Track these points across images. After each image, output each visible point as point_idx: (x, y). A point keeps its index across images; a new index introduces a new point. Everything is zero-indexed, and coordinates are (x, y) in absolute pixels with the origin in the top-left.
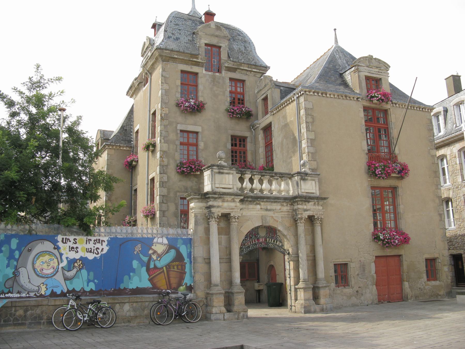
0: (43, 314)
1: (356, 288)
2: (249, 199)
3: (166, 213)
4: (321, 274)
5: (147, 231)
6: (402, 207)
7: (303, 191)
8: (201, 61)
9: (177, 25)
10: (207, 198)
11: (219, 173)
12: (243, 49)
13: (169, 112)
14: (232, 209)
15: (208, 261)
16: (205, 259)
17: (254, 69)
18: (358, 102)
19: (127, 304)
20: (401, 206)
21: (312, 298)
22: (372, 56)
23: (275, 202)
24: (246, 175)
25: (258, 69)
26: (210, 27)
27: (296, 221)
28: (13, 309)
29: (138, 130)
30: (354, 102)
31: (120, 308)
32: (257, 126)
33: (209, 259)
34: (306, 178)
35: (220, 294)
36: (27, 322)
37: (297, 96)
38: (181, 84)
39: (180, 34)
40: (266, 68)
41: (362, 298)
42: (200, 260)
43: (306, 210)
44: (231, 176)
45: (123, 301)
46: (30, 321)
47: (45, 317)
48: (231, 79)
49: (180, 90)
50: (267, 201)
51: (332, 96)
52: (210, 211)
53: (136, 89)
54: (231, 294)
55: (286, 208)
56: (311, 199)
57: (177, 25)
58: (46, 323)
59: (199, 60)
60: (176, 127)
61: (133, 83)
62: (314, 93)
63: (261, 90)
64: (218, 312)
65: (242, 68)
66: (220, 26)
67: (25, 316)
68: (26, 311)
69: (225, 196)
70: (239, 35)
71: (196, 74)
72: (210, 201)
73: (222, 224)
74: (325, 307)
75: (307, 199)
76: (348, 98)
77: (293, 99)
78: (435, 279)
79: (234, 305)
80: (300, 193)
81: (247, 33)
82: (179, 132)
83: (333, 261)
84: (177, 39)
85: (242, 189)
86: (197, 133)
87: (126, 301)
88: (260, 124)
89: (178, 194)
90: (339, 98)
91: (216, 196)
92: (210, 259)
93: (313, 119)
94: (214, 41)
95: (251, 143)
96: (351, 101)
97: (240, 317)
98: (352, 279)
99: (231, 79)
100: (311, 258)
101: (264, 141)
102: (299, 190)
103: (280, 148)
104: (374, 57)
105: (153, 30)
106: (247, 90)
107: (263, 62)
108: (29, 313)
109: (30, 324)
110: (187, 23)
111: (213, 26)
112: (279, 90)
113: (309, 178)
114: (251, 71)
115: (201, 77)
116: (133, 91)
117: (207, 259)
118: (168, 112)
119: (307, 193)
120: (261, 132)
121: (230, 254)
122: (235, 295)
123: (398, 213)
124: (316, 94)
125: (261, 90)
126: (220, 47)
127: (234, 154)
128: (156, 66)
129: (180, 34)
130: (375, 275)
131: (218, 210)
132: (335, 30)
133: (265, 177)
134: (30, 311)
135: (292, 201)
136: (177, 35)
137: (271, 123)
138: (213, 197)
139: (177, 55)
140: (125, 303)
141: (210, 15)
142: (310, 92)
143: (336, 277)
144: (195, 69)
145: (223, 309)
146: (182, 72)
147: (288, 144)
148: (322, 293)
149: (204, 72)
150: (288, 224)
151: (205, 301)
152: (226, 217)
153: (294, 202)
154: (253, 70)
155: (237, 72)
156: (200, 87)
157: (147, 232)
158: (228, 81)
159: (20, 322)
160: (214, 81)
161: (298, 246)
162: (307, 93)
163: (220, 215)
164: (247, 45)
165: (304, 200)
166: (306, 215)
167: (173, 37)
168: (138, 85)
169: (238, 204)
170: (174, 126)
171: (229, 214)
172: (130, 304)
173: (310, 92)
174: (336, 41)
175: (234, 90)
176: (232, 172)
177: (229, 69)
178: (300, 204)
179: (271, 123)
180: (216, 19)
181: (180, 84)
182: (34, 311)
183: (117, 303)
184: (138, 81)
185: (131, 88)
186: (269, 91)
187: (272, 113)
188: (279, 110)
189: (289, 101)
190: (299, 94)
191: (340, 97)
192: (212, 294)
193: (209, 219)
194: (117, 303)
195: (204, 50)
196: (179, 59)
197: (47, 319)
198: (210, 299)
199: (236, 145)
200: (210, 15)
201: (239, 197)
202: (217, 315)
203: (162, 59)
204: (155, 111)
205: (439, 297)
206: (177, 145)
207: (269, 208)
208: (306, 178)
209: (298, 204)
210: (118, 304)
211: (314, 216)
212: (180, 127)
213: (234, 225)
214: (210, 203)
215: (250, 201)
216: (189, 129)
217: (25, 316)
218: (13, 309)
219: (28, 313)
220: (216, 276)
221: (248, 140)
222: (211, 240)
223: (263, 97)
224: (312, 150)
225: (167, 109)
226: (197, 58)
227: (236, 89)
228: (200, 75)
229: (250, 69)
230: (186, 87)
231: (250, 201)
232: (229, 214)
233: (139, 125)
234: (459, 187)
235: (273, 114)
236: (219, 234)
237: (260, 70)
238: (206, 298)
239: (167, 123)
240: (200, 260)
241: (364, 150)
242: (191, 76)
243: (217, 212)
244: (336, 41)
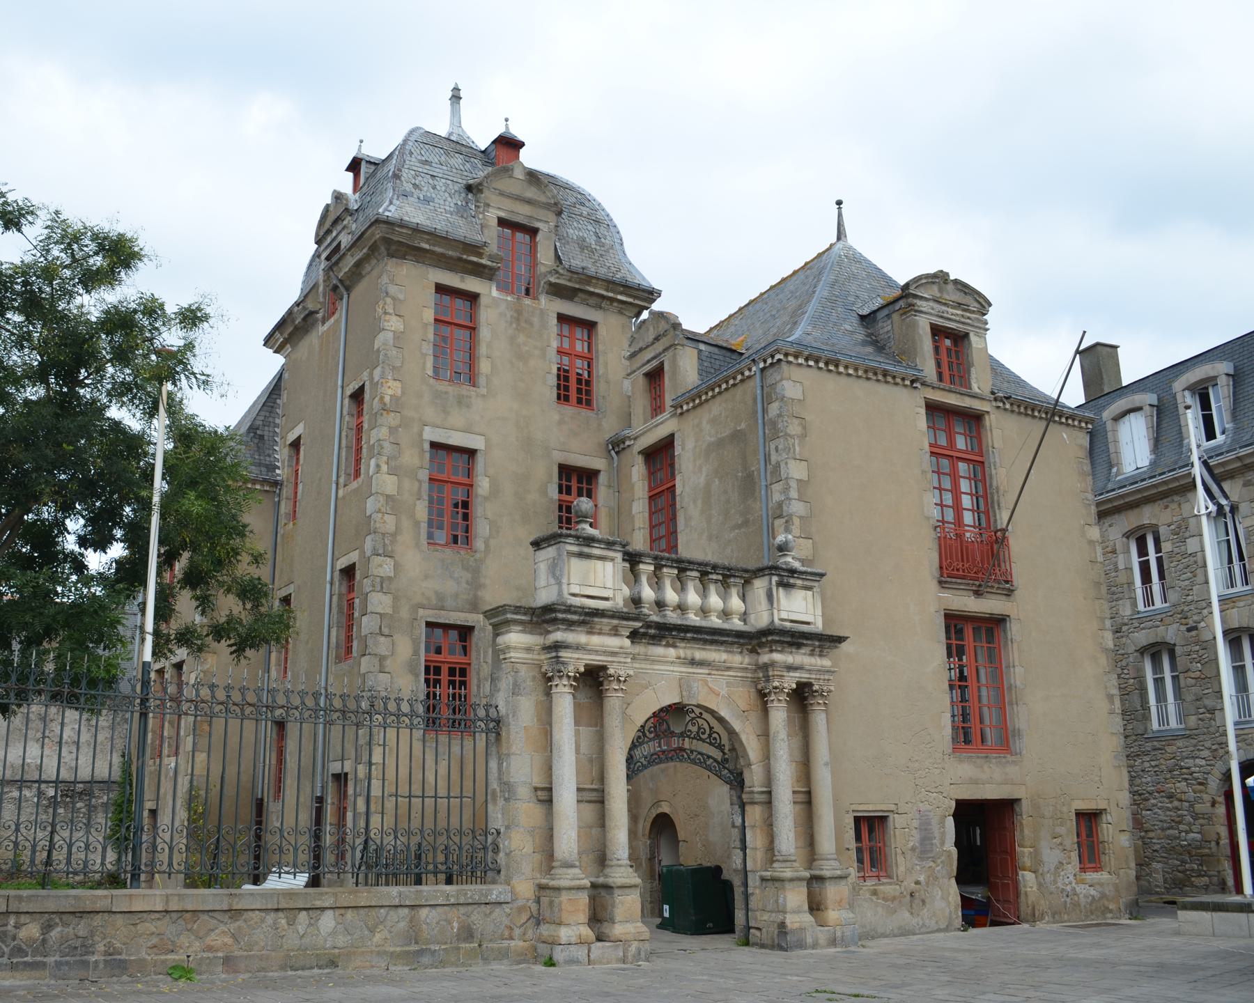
0: (97, 938)
1: (909, 884)
2: (656, 631)
3: (388, 662)
4: (826, 844)
5: (398, 705)
6: (1019, 670)
7: (784, 615)
8: (489, 263)
9: (426, 162)
10: (547, 622)
11: (581, 555)
12: (592, 240)
13: (403, 393)
14: (613, 654)
15: (546, 796)
16: (536, 789)
17: (621, 293)
18: (916, 393)
19: (329, 913)
20: (1017, 670)
21: (806, 907)
22: (947, 274)
23: (712, 642)
24: (641, 566)
25: (631, 296)
26: (511, 177)
27: (765, 695)
28: (12, 921)
29: (299, 437)
30: (905, 391)
31: (310, 925)
32: (627, 443)
33: (550, 789)
34: (792, 581)
35: (579, 888)
36: (51, 960)
37: (762, 365)
38: (436, 320)
39: (434, 188)
40: (651, 294)
41: (925, 912)
42: (524, 792)
43: (790, 668)
44: (609, 565)
45: (318, 904)
46: (57, 958)
47: (101, 947)
48: (562, 318)
49: (431, 336)
50: (693, 639)
51: (851, 371)
52: (558, 657)
53: (296, 328)
54: (603, 893)
55: (738, 659)
56: (807, 639)
57: (426, 162)
58: (101, 966)
59: (484, 261)
60: (421, 435)
61: (290, 312)
62: (807, 359)
63: (641, 350)
64: (573, 940)
65: (592, 289)
66: (533, 177)
67: (44, 941)
68: (47, 928)
69: (596, 619)
70: (582, 204)
71: (473, 298)
72: (558, 629)
73: (584, 697)
74: (839, 934)
75: (795, 638)
76: (889, 379)
77: (747, 373)
78: (1097, 869)
79: (613, 921)
80: (776, 620)
81: (599, 199)
82: (427, 446)
83: (854, 807)
84: (427, 201)
85: (636, 601)
86: (471, 453)
87: (327, 904)
88: (635, 439)
89: (421, 612)
90: (868, 379)
91: (575, 617)
92: (550, 790)
93: (804, 428)
94: (522, 213)
95: (609, 486)
96: (895, 389)
97: (630, 955)
98: (900, 859)
99: (562, 318)
100: (801, 798)
101: (646, 483)
102: (775, 612)
103: (699, 503)
104: (952, 277)
105: (351, 175)
106: (601, 347)
107: (644, 279)
108: (55, 934)
109: (58, 965)
110: (452, 161)
111: (519, 174)
112: (696, 351)
113: (799, 582)
114: (612, 300)
115: (487, 307)
116: (286, 335)
117: (543, 789)
118: (399, 392)
119: (792, 621)
120: (640, 460)
121: (602, 778)
122: (617, 892)
123: (1010, 688)
124: (811, 363)
125: (641, 350)
126: (533, 232)
127: (564, 514)
128: (368, 268)
129: (434, 188)
130: (954, 851)
131: (576, 656)
132: (839, 203)
133: (688, 573)
134: (59, 929)
135: (755, 642)
136: (427, 191)
137: (672, 436)
138: (564, 621)
139: (428, 242)
140: (323, 909)
141: (509, 144)
142: (796, 357)
143: (859, 850)
144: (471, 284)
145: (586, 932)
146: (441, 289)
147: (725, 492)
148: (832, 892)
149: (495, 293)
150: (743, 705)
151: (534, 907)
152: (593, 680)
153: (761, 645)
154: (620, 297)
155: (576, 299)
156: (484, 333)
157: (399, 709)
158: (554, 321)
159: (28, 959)
160: (518, 316)
161: (769, 764)
162: (791, 359)
163: (582, 669)
164: (603, 230)
165: (789, 639)
166: (790, 681)
167: (416, 192)
168: (304, 319)
169: (627, 642)
170: (415, 430)
171: (604, 668)
172: (338, 912)
173: (796, 357)
174: (841, 234)
175: (566, 345)
176: (611, 554)
177: (558, 291)
178: (777, 651)
179: (672, 436)
180: (528, 158)
181: (432, 321)
182: (70, 930)
183: (301, 909)
184: (304, 308)
185: (280, 326)
186: (669, 354)
187: (679, 411)
188: (701, 404)
189: (734, 378)
190: (769, 361)
191: (870, 375)
192: (558, 889)
193: (550, 679)
194: (301, 909)
195: (495, 235)
196: (433, 253)
197: (107, 953)
198: (551, 903)
199: (569, 492)
200: (509, 144)
201: (631, 623)
202: (572, 948)
203: (388, 250)
204: (362, 388)
205: (1109, 915)
206: (420, 482)
207: (699, 655)
208: (792, 581)
209: (771, 651)
210: (304, 913)
211: (810, 685)
212: (430, 434)
213: (614, 701)
214: (558, 636)
215: (653, 637)
216: (451, 442)
217: (44, 941)
218: (12, 921)
219: (53, 934)
220: (568, 840)
221: (602, 478)
222: (556, 736)
223: (648, 368)
224: (1192, 546)
225: (398, 384)
226: (480, 255)
227: (572, 345)
228: (483, 301)
229: (611, 295)
230: (446, 330)
231: (653, 637)
232: (604, 668)
233: (301, 426)
234: (1125, 628)
235: (681, 414)
236: (577, 723)
237: (635, 297)
238: (538, 901)
239: (397, 422)
240: (524, 792)
241: (928, 518)
242: (459, 303)
243: (576, 662)
244: (841, 234)
